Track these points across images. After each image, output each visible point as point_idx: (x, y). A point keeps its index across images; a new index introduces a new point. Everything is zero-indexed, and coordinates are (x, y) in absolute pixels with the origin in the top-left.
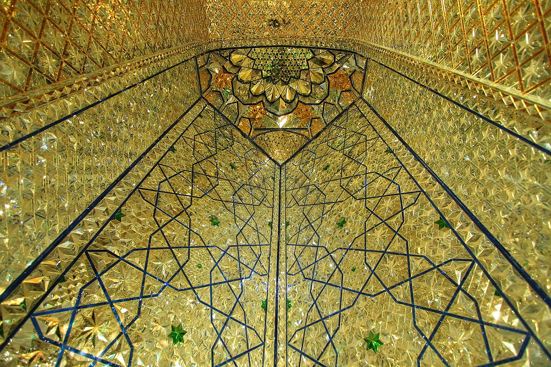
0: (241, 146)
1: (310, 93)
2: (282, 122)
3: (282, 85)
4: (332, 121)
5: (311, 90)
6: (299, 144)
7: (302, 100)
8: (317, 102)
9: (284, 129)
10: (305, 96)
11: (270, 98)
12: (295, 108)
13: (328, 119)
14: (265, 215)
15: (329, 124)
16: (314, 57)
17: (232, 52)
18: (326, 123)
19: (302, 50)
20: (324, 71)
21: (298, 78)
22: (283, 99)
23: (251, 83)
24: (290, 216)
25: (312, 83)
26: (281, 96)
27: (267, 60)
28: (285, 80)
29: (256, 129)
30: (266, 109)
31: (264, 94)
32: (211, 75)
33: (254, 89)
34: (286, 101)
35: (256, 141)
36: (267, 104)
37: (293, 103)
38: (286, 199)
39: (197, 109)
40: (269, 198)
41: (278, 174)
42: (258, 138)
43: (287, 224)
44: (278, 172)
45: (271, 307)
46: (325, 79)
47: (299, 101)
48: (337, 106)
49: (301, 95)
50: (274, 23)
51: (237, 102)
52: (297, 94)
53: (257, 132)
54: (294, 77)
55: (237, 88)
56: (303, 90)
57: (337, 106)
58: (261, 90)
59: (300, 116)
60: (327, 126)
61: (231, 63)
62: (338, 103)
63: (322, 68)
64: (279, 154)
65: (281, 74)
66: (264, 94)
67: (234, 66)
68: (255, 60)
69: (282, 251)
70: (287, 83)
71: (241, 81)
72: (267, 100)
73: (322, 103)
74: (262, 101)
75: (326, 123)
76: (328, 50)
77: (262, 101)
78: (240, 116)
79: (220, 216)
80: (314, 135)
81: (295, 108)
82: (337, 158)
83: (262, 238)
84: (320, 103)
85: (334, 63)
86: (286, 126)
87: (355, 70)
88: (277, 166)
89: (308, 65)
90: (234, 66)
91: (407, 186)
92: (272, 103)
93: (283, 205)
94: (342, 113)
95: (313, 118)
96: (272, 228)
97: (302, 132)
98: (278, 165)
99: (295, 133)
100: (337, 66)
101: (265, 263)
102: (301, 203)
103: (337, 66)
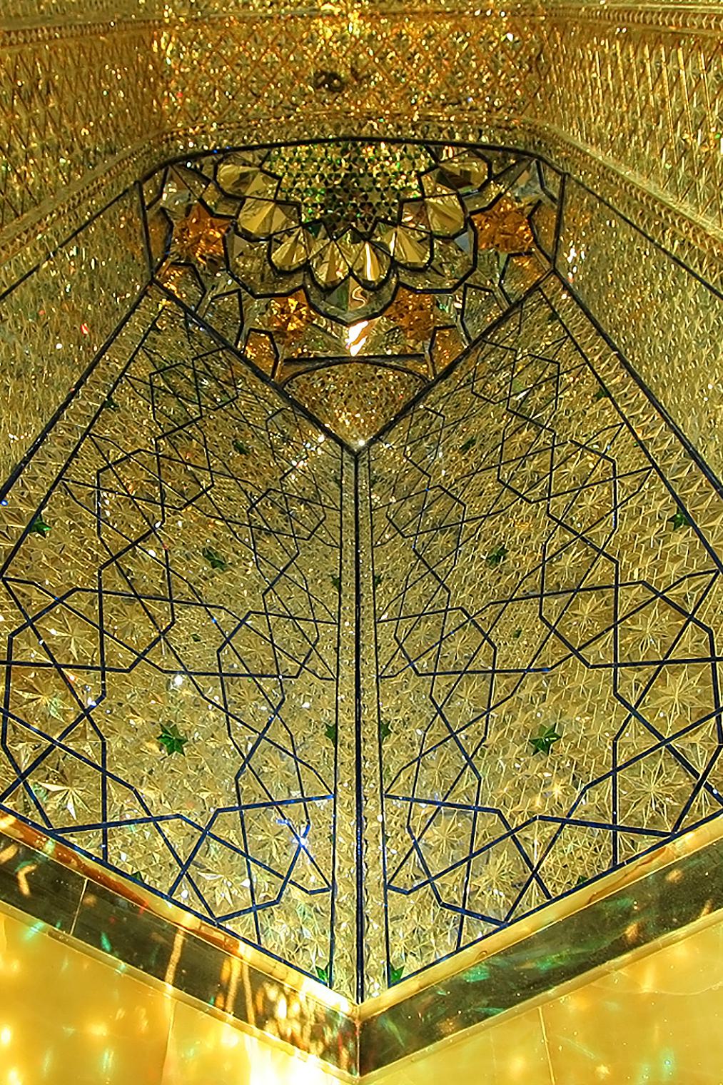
0: (256, 401)
1: (430, 262)
2: (355, 339)
3: (354, 241)
4: (484, 334)
5: (432, 254)
6: (402, 396)
7: (406, 281)
8: (448, 285)
9: (362, 360)
10: (415, 270)
11: (322, 276)
12: (390, 304)
13: (475, 330)
14: (320, 562)
15: (477, 341)
16: (436, 167)
17: (221, 161)
18: (468, 338)
19: (405, 150)
20: (462, 203)
21: (397, 222)
22: (356, 278)
23: (273, 240)
24: (384, 563)
25: (432, 236)
26: (351, 270)
27: (306, 170)
28: (362, 229)
29: (290, 361)
30: (312, 306)
31: (306, 267)
32: (171, 223)
33: (278, 256)
34: (366, 285)
35: (294, 390)
36: (314, 292)
37: (386, 289)
38: (372, 527)
39: (145, 311)
40: (326, 648)
41: (349, 473)
42: (297, 381)
43: (377, 580)
44: (349, 471)
45: (346, 735)
46: (465, 226)
47: (399, 284)
48: (498, 294)
49: (403, 266)
50: (328, 81)
51: (239, 291)
52: (395, 265)
53: (292, 369)
54: (385, 221)
55: (236, 254)
56: (411, 254)
57: (498, 294)
58: (296, 261)
59: (403, 322)
60: (474, 344)
61: (219, 188)
62: (500, 285)
63: (459, 196)
64: (350, 423)
65: (350, 210)
66: (306, 267)
67: (227, 197)
68: (280, 179)
69: (368, 632)
70: (367, 238)
71: (248, 236)
72: (315, 284)
73: (461, 288)
74: (303, 287)
75: (468, 338)
76: (472, 147)
77: (303, 287)
78: (246, 328)
79: (225, 551)
80: (440, 369)
81: (390, 304)
82: (493, 420)
83: (308, 777)
84: (456, 287)
85: (487, 183)
86: (367, 350)
87: (540, 202)
88: (345, 454)
89: (421, 186)
90: (227, 197)
91: (630, 460)
92: (328, 290)
93: (365, 541)
94: (509, 311)
95: (436, 328)
96: (340, 591)
97: (410, 364)
98: (351, 452)
99: (391, 367)
100: (494, 190)
101: (330, 660)
102: (410, 530)
103: (494, 190)
